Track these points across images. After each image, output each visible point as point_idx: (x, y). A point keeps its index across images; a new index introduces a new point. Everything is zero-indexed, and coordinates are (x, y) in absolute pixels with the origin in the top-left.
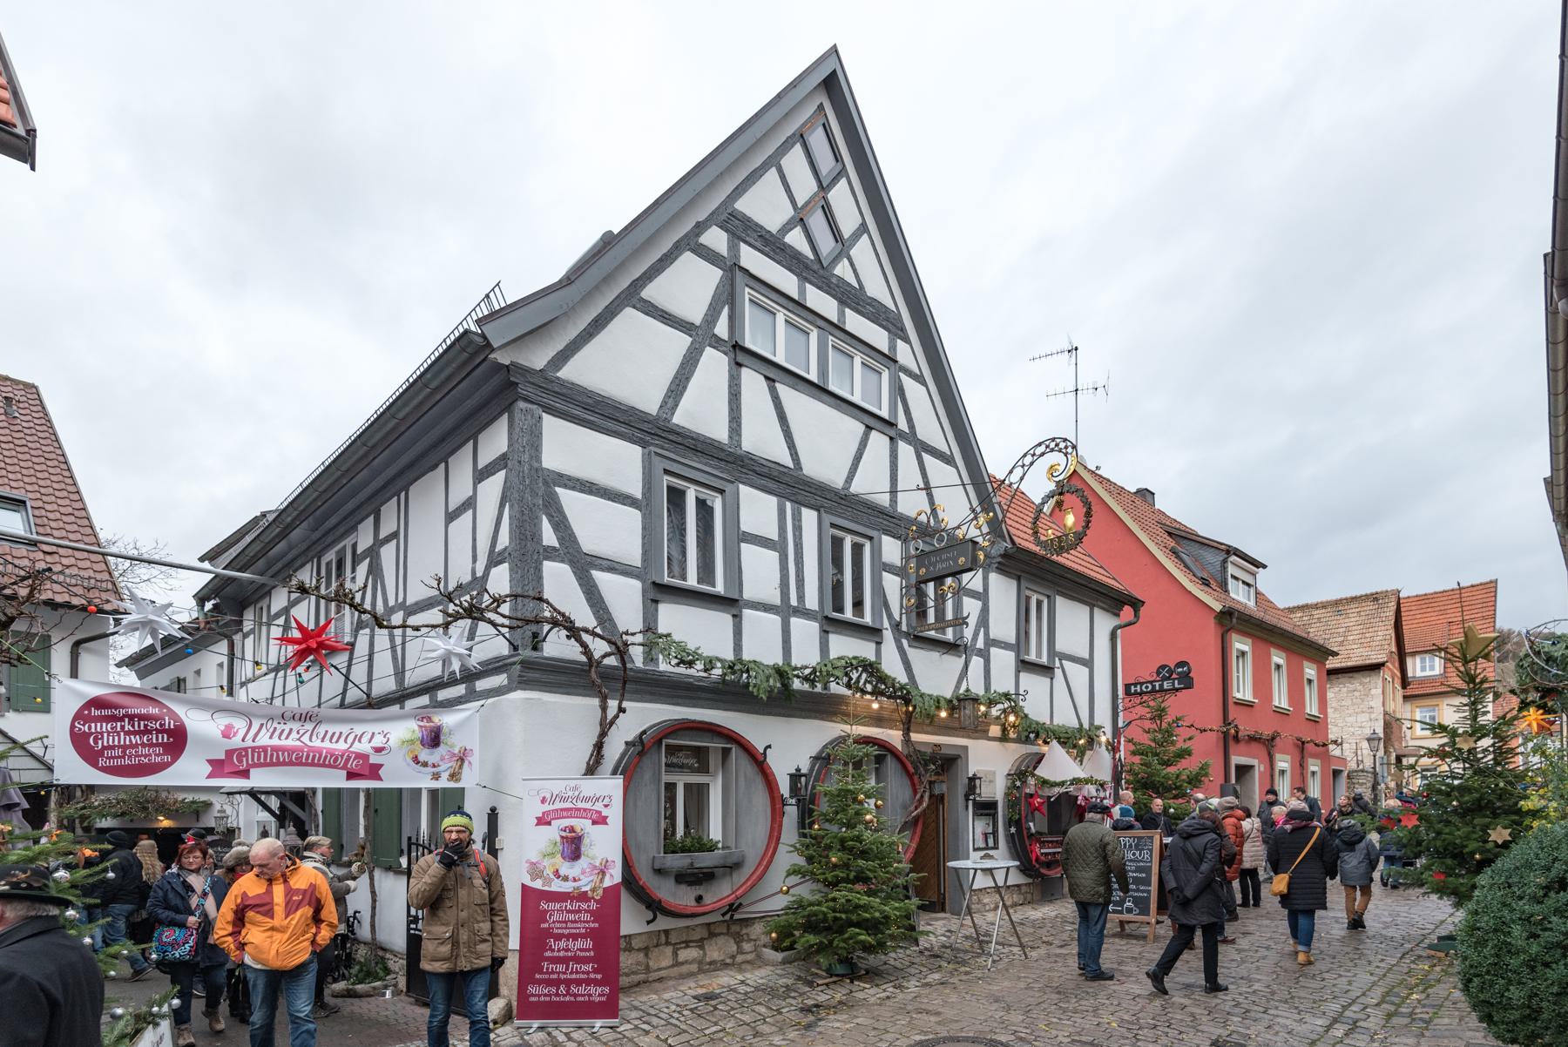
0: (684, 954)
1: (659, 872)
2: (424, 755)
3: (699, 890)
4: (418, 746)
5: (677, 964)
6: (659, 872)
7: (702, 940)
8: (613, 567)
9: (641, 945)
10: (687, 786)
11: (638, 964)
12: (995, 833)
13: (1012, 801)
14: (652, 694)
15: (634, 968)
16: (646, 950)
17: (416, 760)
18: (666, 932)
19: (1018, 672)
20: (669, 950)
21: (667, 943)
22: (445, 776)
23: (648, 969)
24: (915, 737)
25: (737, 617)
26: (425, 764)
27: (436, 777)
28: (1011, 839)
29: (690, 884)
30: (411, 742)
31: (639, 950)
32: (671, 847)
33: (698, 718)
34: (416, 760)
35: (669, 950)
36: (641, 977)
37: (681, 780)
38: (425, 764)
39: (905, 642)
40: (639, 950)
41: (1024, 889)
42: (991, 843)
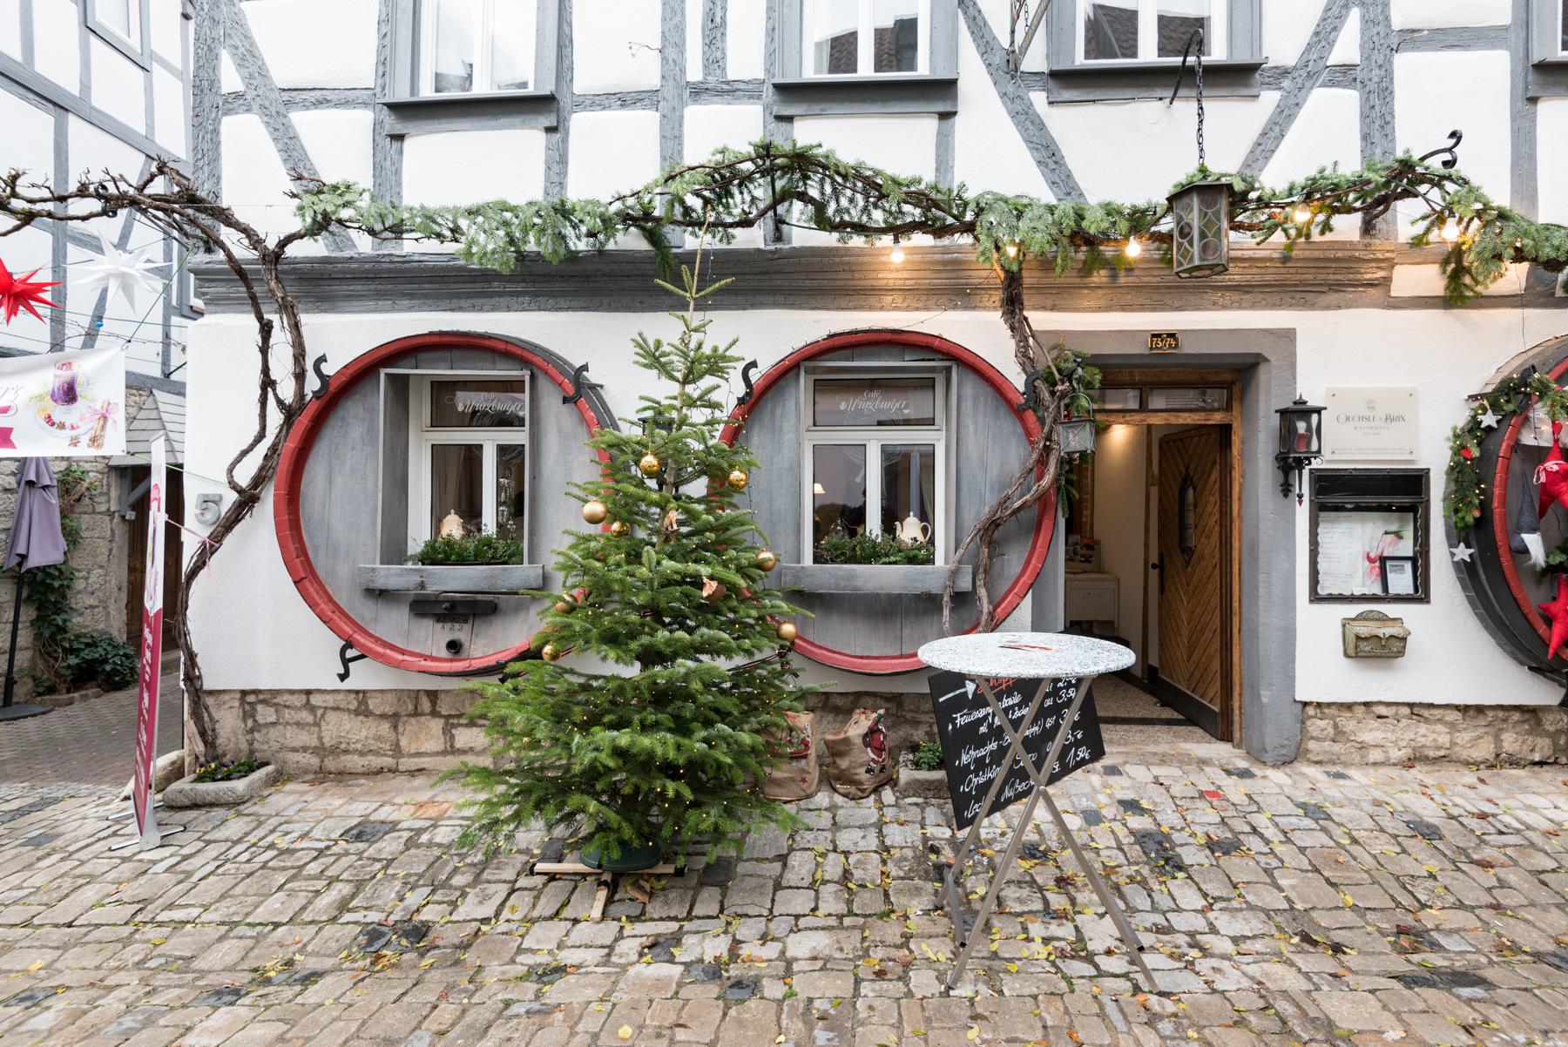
0: (464, 737)
1: (380, 595)
2: (60, 412)
3: (460, 633)
4: (49, 403)
5: (451, 750)
6: (380, 595)
7: (396, 716)
8: (321, 98)
9: (389, 710)
10: (503, 450)
11: (378, 738)
12: (1420, 562)
13: (1467, 474)
14: (411, 296)
15: (375, 746)
16: (394, 719)
17: (49, 420)
18: (433, 695)
19: (125, 251)
20: (436, 725)
21: (434, 713)
22: (85, 440)
23: (397, 751)
24: (1039, 319)
25: (1412, 39)
26: (62, 426)
27: (75, 442)
28: (1467, 572)
29: (440, 618)
30: (41, 398)
31: (383, 716)
32: (394, 550)
33: (454, 328)
34: (49, 420)
35: (436, 725)
36: (387, 761)
37: (490, 441)
38: (62, 426)
39: (1038, 99)
40: (383, 716)
41: (1550, 722)
42: (1401, 581)
